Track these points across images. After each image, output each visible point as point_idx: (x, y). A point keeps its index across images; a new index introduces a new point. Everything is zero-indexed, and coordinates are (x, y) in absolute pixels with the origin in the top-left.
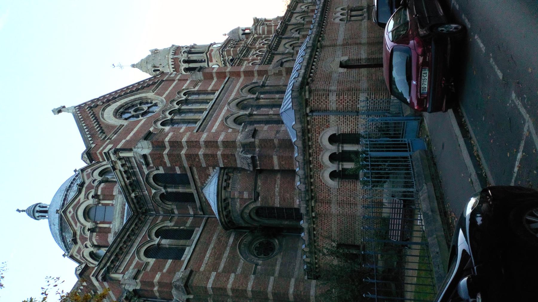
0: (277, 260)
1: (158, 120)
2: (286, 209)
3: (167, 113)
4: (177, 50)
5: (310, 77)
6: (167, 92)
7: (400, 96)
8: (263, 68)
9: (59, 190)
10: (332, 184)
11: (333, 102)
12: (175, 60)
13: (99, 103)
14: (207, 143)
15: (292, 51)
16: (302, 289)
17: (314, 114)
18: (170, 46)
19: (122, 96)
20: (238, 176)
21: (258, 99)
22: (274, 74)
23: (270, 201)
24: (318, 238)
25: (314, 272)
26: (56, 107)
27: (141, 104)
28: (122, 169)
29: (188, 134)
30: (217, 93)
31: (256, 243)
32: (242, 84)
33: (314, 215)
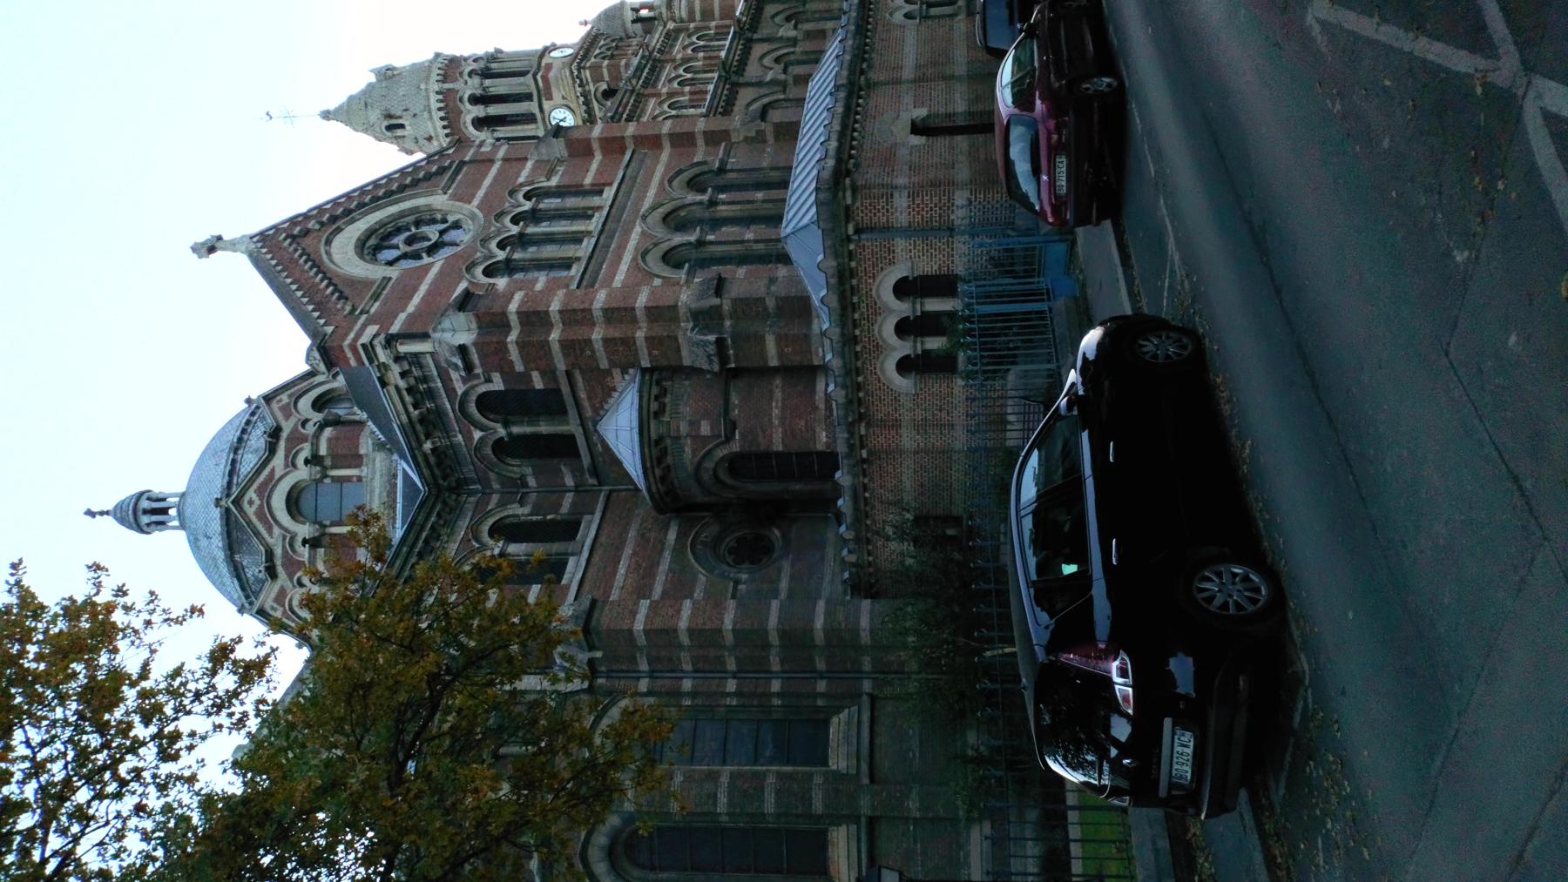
0: (780, 570)
1: (474, 264)
2: (797, 454)
3: (493, 245)
4: (450, 67)
5: (851, 157)
6: (481, 193)
7: (1023, 200)
8: (718, 123)
9: (210, 451)
10: (902, 384)
11: (901, 210)
12: (448, 97)
13: (312, 224)
14: (611, 314)
15: (783, 77)
16: (840, 617)
17: (864, 236)
18: (431, 56)
19: (365, 205)
20: (684, 386)
21: (713, 203)
22: (746, 139)
23: (760, 439)
24: (873, 507)
25: (864, 585)
26: (201, 240)
27: (418, 224)
28: (402, 384)
29: (561, 293)
30: (609, 193)
31: (730, 540)
32: (668, 167)
33: (864, 454)
